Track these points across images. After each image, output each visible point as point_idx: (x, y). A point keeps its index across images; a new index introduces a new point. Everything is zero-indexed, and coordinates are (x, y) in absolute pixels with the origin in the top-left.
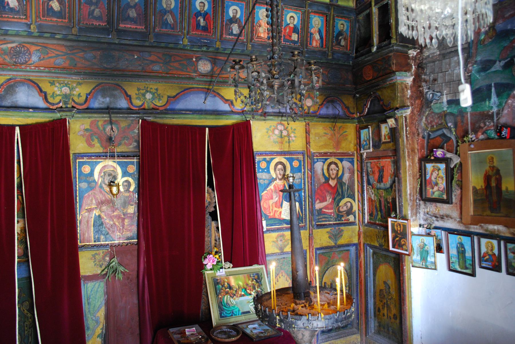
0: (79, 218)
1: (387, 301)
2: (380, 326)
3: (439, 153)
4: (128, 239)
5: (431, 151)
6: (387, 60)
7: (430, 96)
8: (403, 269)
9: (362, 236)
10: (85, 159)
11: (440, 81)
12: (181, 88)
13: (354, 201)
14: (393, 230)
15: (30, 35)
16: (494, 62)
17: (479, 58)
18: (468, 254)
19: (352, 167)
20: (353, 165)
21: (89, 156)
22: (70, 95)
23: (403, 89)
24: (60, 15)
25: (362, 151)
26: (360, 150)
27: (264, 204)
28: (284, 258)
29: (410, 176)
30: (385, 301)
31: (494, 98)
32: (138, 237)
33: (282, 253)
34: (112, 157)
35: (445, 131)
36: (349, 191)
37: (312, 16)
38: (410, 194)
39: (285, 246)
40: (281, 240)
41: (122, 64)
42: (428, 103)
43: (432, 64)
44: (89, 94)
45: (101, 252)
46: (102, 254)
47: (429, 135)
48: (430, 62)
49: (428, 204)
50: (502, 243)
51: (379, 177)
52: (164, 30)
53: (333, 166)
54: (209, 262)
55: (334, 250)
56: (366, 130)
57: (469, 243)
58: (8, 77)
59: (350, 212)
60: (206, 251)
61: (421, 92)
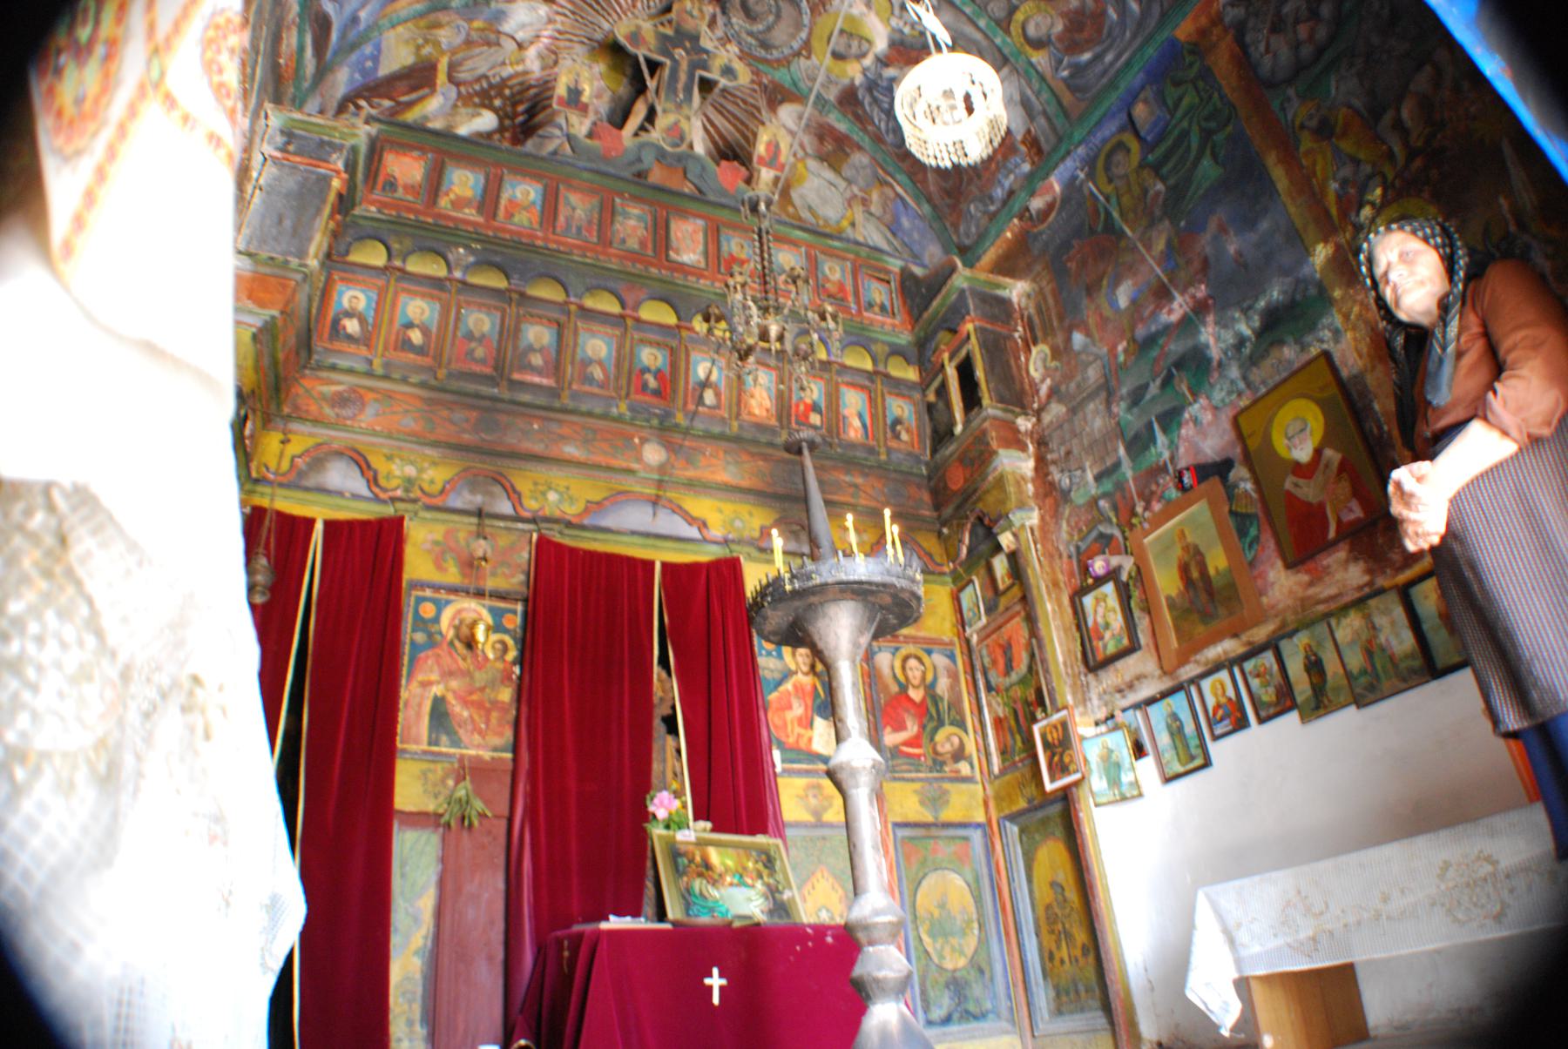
0: (404, 694)
1: (1063, 925)
2: (1058, 995)
3: (1098, 566)
4: (495, 749)
5: (1085, 570)
6: (981, 438)
7: (1066, 482)
8: (1077, 817)
9: (992, 804)
10: (428, 593)
11: (1075, 451)
12: (611, 489)
13: (966, 731)
14: (1046, 745)
15: (370, 374)
16: (1145, 387)
17: (1124, 391)
18: (1189, 728)
19: (952, 665)
20: (954, 661)
21: (436, 588)
22: (416, 479)
23: (1018, 483)
24: (421, 351)
25: (968, 631)
26: (964, 630)
27: (773, 718)
28: (824, 838)
29: (1057, 628)
30: (1060, 927)
31: (1161, 438)
32: (515, 749)
33: (820, 824)
34: (480, 594)
35: (1102, 528)
36: (953, 713)
37: (844, 389)
38: (1065, 664)
39: (825, 809)
40: (815, 796)
41: (512, 440)
42: (1065, 495)
43: (1059, 432)
44: (448, 482)
45: (440, 768)
46: (440, 772)
47: (1078, 548)
48: (1055, 430)
49: (1102, 674)
50: (1236, 671)
51: (1006, 665)
52: (587, 388)
53: (912, 663)
54: (662, 805)
55: (934, 832)
56: (969, 589)
57: (1185, 703)
58: (319, 440)
59: (959, 755)
60: (655, 781)
61: (1052, 485)
